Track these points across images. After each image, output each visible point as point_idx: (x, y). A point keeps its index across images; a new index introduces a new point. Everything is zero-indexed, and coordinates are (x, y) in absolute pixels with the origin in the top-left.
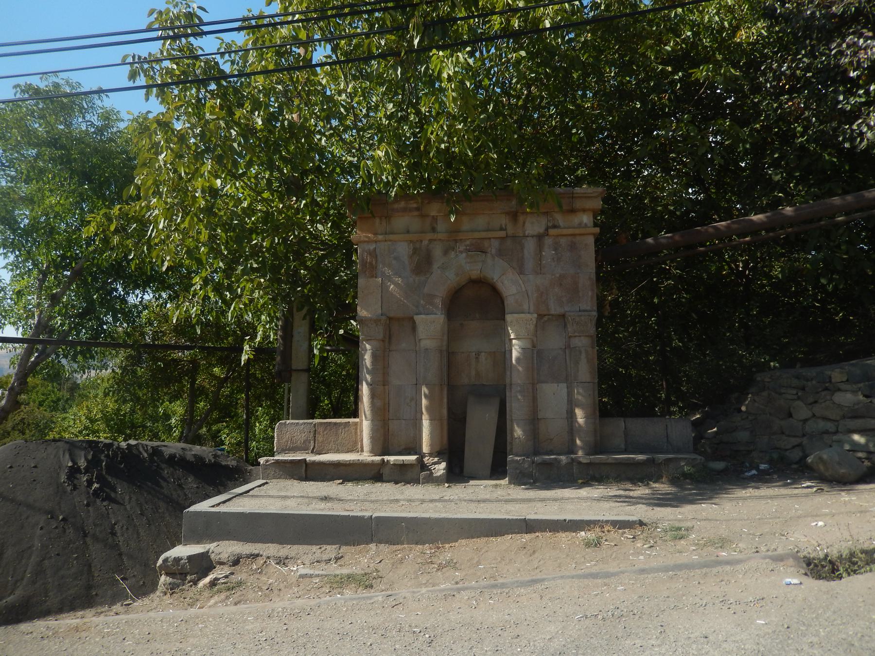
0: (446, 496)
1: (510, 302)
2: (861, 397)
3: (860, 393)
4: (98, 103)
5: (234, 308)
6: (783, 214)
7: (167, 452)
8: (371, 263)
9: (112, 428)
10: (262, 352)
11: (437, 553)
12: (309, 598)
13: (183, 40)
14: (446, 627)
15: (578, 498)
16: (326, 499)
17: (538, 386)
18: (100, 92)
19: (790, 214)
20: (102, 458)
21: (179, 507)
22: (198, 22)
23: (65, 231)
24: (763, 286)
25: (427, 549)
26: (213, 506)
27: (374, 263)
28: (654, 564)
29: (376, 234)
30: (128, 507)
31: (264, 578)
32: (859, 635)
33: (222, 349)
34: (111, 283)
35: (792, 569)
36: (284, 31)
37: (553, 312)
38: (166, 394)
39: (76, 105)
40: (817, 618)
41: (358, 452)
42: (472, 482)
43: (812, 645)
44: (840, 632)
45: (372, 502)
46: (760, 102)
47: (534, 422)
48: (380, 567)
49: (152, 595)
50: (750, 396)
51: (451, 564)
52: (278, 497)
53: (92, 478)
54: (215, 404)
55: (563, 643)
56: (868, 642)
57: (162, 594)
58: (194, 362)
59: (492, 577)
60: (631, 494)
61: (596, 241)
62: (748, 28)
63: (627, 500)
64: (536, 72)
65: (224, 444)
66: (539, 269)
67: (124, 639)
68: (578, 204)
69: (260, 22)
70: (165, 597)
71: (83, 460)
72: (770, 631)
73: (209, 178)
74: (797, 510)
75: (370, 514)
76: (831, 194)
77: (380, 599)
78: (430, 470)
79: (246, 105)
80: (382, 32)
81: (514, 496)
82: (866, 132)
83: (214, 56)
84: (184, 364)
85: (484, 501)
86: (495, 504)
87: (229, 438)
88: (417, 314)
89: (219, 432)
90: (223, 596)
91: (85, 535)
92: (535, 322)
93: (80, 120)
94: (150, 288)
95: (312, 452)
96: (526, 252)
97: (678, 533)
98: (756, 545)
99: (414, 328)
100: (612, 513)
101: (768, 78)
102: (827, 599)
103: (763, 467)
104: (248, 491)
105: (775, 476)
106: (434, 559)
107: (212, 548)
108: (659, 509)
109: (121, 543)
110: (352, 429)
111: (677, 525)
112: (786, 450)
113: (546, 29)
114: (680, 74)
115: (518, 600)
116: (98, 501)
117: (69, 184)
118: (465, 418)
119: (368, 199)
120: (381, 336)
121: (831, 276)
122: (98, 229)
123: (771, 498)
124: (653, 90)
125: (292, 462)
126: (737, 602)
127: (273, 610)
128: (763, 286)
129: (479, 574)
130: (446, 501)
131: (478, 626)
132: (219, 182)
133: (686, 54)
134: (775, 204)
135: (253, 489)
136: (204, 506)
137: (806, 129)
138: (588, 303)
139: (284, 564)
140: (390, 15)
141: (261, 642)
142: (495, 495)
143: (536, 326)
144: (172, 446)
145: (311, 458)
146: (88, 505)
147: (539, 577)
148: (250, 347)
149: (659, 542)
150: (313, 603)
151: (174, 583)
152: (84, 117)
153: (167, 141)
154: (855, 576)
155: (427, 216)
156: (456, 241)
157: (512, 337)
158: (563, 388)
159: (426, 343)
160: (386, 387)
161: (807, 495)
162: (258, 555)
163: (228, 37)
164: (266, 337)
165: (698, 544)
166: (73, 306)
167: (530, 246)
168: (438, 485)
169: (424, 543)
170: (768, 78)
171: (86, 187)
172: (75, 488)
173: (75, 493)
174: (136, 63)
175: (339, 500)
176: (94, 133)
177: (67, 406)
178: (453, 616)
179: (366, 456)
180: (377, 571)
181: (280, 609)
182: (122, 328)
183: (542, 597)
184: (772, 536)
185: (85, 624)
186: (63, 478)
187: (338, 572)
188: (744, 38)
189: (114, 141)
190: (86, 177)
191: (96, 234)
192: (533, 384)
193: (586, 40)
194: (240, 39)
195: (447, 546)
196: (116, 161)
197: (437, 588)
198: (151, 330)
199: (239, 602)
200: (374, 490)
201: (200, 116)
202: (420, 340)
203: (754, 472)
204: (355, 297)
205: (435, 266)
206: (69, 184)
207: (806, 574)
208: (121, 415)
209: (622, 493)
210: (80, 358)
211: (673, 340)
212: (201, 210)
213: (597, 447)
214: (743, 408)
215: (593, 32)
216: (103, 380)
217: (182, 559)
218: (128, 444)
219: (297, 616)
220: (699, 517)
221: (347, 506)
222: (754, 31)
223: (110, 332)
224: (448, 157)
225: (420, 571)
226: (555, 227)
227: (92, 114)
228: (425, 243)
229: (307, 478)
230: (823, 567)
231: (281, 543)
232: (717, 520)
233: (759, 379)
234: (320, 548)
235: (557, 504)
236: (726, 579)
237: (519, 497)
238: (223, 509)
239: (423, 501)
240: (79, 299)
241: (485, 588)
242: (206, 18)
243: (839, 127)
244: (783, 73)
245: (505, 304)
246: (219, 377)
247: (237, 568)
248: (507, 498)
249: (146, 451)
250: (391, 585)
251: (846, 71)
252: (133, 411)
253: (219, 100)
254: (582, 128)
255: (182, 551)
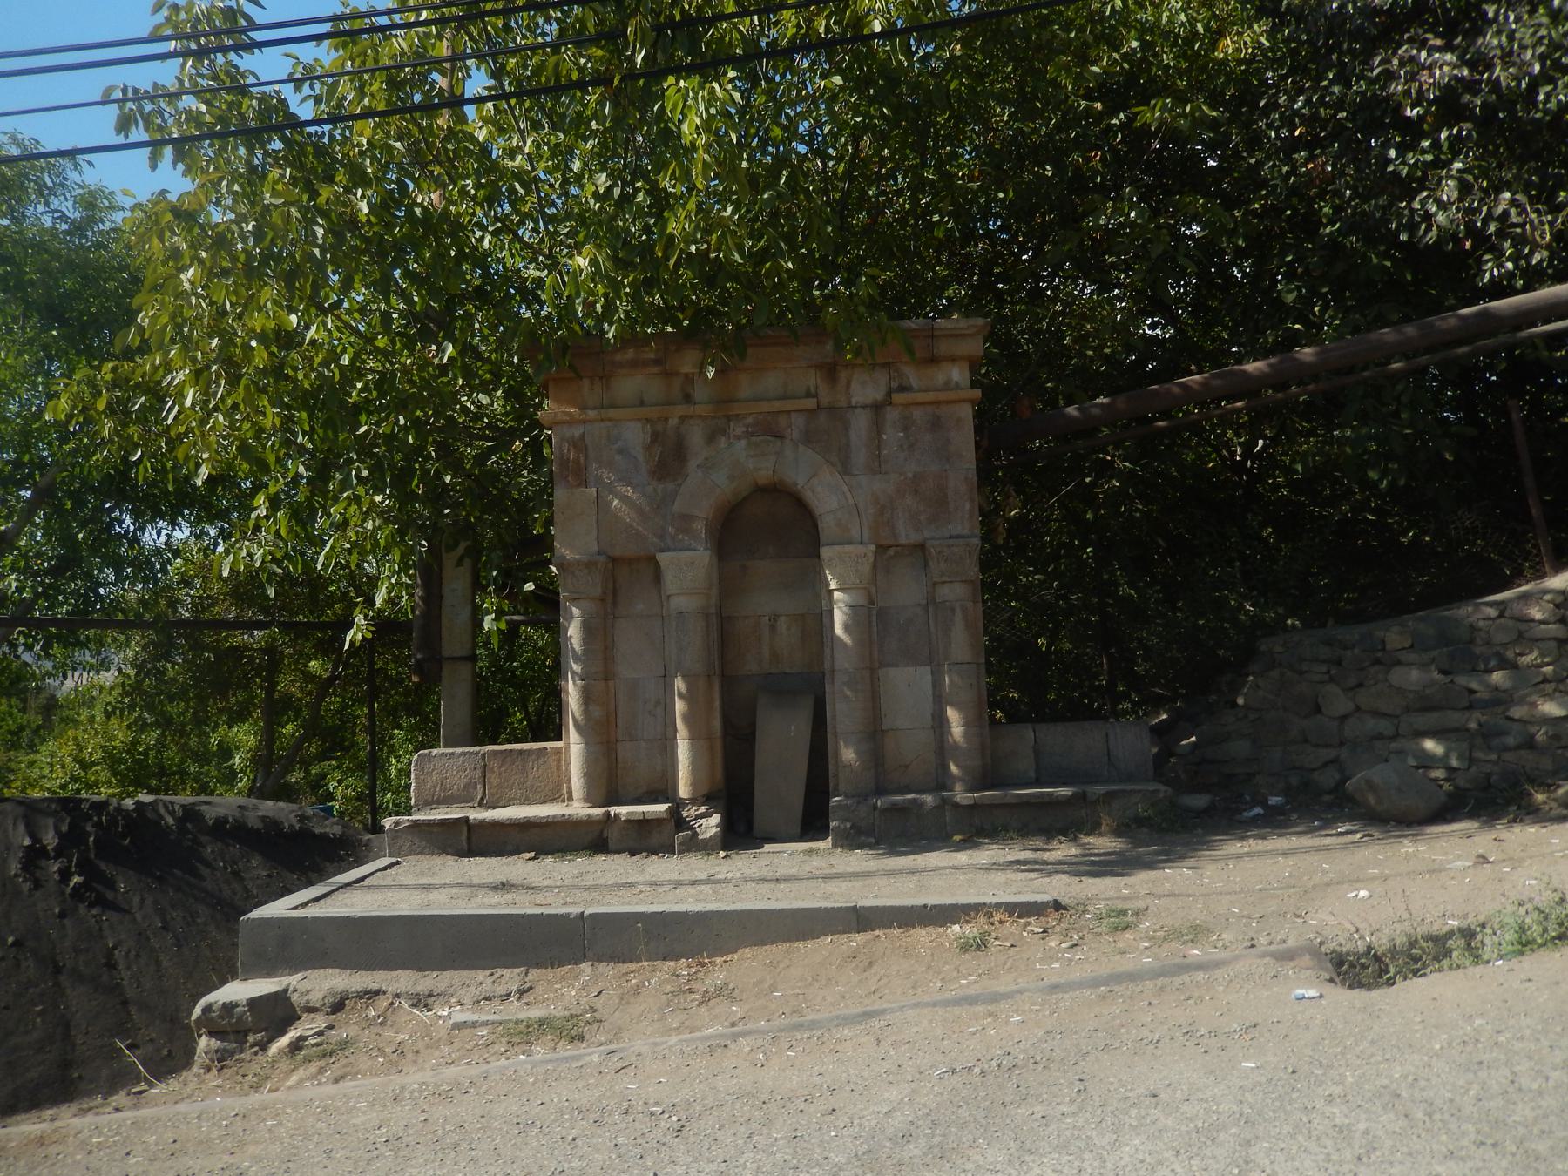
0: (719, 873)
1: (827, 525)
2: (1436, 675)
3: (1433, 667)
4: (74, 176)
5: (332, 548)
6: (1296, 359)
7: (210, 814)
8: (577, 461)
9: (124, 776)
10: (387, 628)
11: (700, 974)
12: (469, 1063)
13: (220, 58)
14: (710, 1101)
15: (953, 867)
16: (503, 887)
17: (881, 672)
18: (72, 154)
19: (1309, 359)
20: (89, 828)
21: (232, 911)
22: (245, 24)
23: (18, 415)
24: (1277, 487)
25: (683, 967)
26: (295, 908)
27: (582, 460)
28: (1076, 974)
29: (583, 408)
30: (138, 916)
31: (389, 1033)
32: (1411, 1078)
33: (323, 626)
34: (111, 510)
35: (1309, 972)
36: (401, 42)
37: (903, 541)
38: (220, 711)
39: (30, 180)
40: (1343, 1054)
41: (563, 801)
42: (768, 847)
43: (1330, 1099)
44: (1379, 1075)
45: (587, 889)
46: (1260, 164)
47: (875, 734)
48: (599, 1003)
49: (184, 1074)
50: (1251, 678)
51: (725, 992)
52: (416, 887)
53: (70, 867)
54: (313, 728)
55: (910, 1118)
56: (1423, 1089)
57: (202, 1071)
58: (271, 650)
59: (797, 1011)
60: (1046, 856)
61: (978, 415)
62: (1239, 34)
63: (1037, 867)
64: (866, 115)
65: (333, 799)
66: (877, 465)
67: (128, 1154)
68: (943, 348)
69: (357, 24)
70: (207, 1076)
71: (51, 834)
72: (1263, 1080)
73: (274, 313)
74: (1325, 872)
75: (579, 910)
76: (1384, 322)
77: (595, 1058)
78: (692, 828)
79: (338, 179)
80: (581, 42)
81: (840, 869)
82: (1436, 214)
83: (276, 87)
84: (252, 656)
85: (787, 879)
86: (809, 884)
87: (342, 787)
88: (662, 551)
89: (324, 777)
90: (313, 1068)
91: (58, 970)
92: (872, 560)
93: (40, 208)
94: (183, 516)
95: (480, 805)
96: (853, 436)
97: (1121, 920)
98: (1251, 934)
99: (657, 577)
100: (1008, 891)
101: (1273, 122)
102: (1363, 1020)
103: (1274, 800)
104: (362, 879)
105: (1294, 816)
106: (694, 986)
107: (294, 983)
108: (1091, 880)
109: (125, 983)
110: (552, 760)
111: (1119, 907)
112: (1314, 770)
113: (874, 36)
114: (1122, 116)
115: (838, 1048)
116: (82, 909)
117: (23, 328)
118: (753, 734)
119: (564, 347)
120: (597, 592)
121: (1386, 465)
122: (74, 407)
123: (1284, 854)
124: (1076, 144)
125: (443, 823)
126: (1214, 1034)
127: (403, 1088)
128: (1277, 487)
129: (773, 1006)
130: (718, 882)
131: (765, 1097)
132: (294, 319)
133: (1131, 77)
134: (1291, 341)
135: (372, 874)
136: (278, 909)
137: (1337, 210)
138: (964, 522)
139: (426, 1006)
140: (596, 14)
141: (378, 1146)
142: (807, 868)
143: (875, 567)
144: (225, 803)
145: (477, 815)
146: (62, 915)
147: (876, 1007)
148: (366, 617)
149: (1088, 937)
150: (474, 1071)
151: (225, 1050)
152: (47, 204)
153: (192, 246)
154: (1415, 979)
155: (677, 374)
156: (728, 418)
157: (833, 586)
158: (924, 675)
159: (680, 603)
160: (611, 683)
161: (1345, 847)
162: (377, 993)
163: (307, 52)
164: (392, 601)
165: (1153, 938)
166: (39, 555)
167: (860, 423)
168: (708, 854)
169: (677, 959)
170: (1273, 122)
171: (54, 333)
172: (37, 885)
173: (38, 894)
174: (130, 100)
175: (528, 888)
176: (67, 232)
177: (37, 741)
178: (720, 1083)
179: (578, 808)
180: (593, 1010)
181: (416, 1086)
182: (134, 593)
183: (879, 1041)
184: (1281, 918)
185: (55, 1131)
186: (14, 867)
187: (522, 1016)
188: (1230, 51)
189: (105, 247)
190: (53, 313)
191: (70, 417)
192: (873, 671)
193: (953, 56)
194: (325, 55)
195: (718, 960)
196: (111, 285)
197: (698, 1034)
198: (188, 595)
199: (343, 1077)
200: (592, 868)
201: (253, 198)
202: (669, 596)
203: (1258, 810)
204: (549, 522)
205: (692, 464)
206: (23, 328)
207: (1331, 981)
208: (140, 753)
209: (1029, 855)
210: (56, 649)
211: (1120, 585)
212: (263, 372)
213: (988, 777)
214: (1240, 701)
215: (966, 42)
216: (101, 688)
217: (237, 1005)
218: (138, 803)
219: (446, 1097)
220: (1159, 891)
221: (540, 898)
222: (1248, 39)
223: (111, 600)
224: (711, 271)
225: (669, 1006)
226: (903, 389)
227: (62, 198)
228: (673, 422)
229: (471, 852)
230: (1364, 967)
231: (420, 969)
232: (1190, 896)
233: (1263, 648)
234: (492, 974)
235: (915, 878)
236: (1196, 994)
237: (849, 869)
238: (313, 912)
239: (678, 884)
240: (50, 540)
241: (780, 1030)
242: (259, 16)
243: (1391, 204)
244: (1297, 113)
245: (820, 526)
246: (320, 677)
247: (341, 1016)
248: (827, 871)
249: (172, 813)
250: (617, 1034)
251: (1399, 107)
252: (161, 745)
253: (288, 170)
254: (949, 214)
255: (238, 991)
